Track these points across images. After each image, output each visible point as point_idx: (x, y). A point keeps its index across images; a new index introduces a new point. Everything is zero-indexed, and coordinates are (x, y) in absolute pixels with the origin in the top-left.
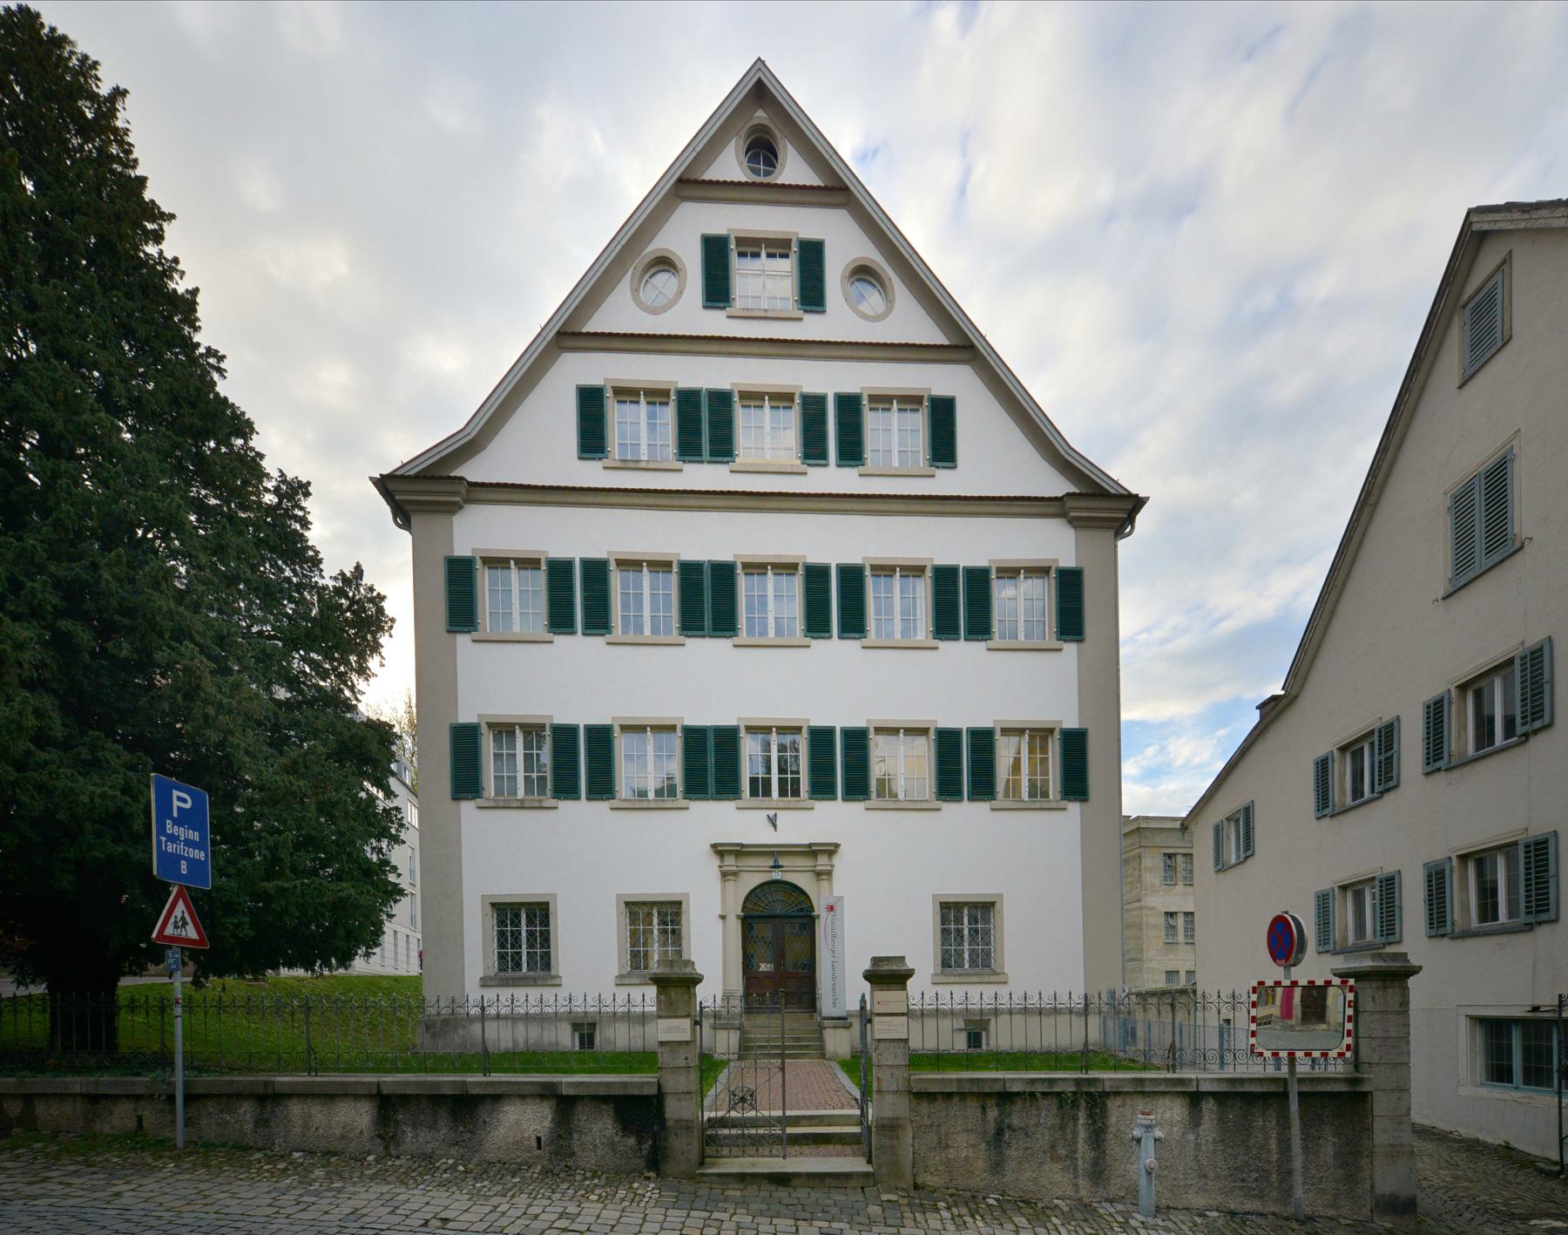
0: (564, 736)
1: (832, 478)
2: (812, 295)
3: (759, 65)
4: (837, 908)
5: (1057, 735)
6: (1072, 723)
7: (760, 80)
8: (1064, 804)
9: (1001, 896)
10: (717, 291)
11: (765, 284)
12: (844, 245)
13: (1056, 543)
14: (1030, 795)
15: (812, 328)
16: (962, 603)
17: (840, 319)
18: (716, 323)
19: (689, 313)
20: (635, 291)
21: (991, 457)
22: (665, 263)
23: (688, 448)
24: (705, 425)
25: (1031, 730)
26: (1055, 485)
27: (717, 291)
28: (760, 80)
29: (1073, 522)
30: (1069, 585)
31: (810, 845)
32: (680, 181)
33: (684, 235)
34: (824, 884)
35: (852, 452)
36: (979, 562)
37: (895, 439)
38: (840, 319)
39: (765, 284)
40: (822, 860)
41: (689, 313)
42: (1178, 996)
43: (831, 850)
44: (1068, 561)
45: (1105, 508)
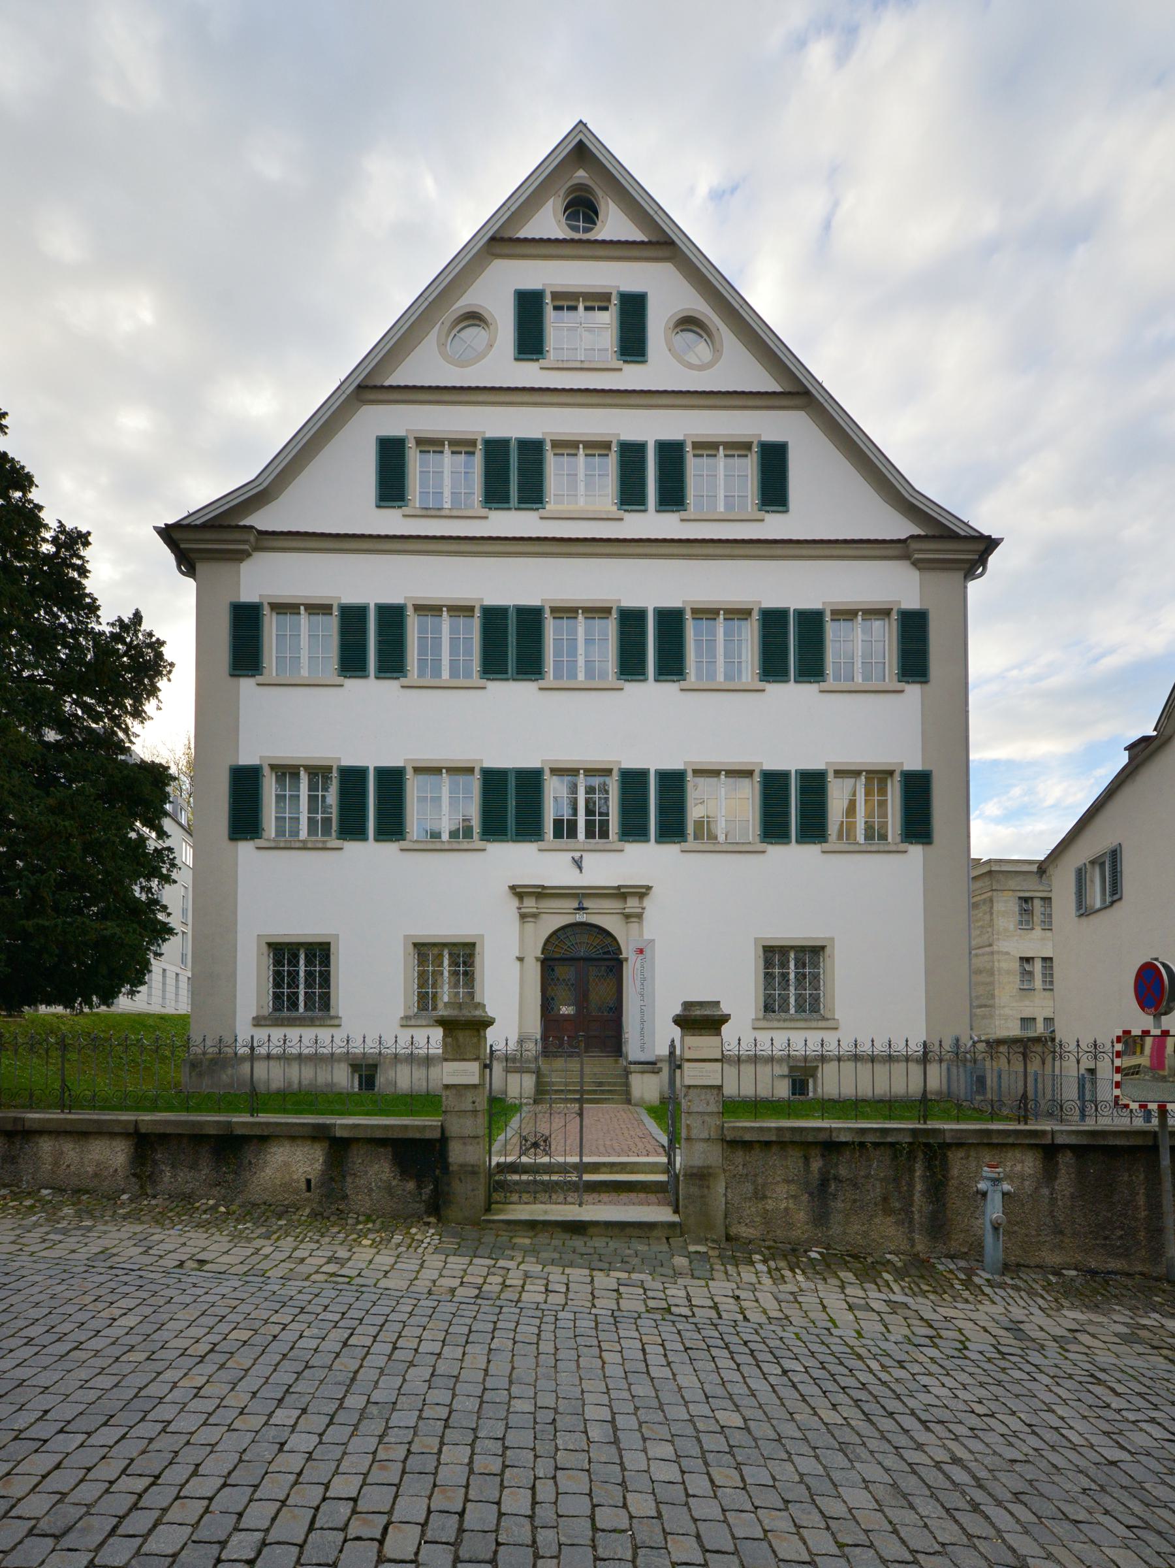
1: (651, 523)
2: (632, 344)
3: (581, 127)
4: (647, 951)
9: (832, 939)
10: (530, 343)
12: (666, 294)
13: (901, 586)
16: (792, 647)
18: (530, 374)
21: (823, 498)
22: (474, 318)
24: (514, 473)
25: (868, 772)
26: (900, 528)
29: (916, 564)
31: (619, 887)
33: (497, 288)
35: (673, 496)
38: (661, 369)
41: (500, 364)
43: (642, 892)
44: (912, 603)
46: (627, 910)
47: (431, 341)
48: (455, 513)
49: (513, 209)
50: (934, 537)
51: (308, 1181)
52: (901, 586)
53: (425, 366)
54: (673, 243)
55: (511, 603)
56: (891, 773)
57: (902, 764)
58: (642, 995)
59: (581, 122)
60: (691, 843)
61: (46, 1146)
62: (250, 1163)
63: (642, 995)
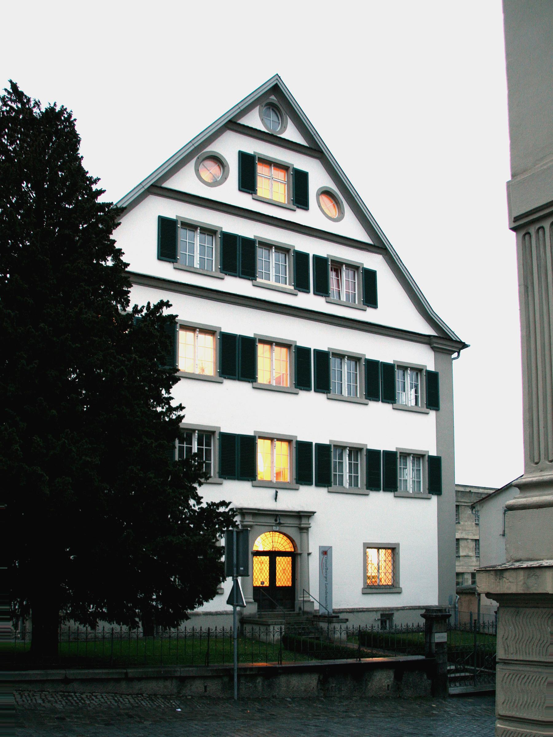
0: (373, 455)
1: (309, 301)
2: (300, 198)
3: (277, 77)
4: (328, 553)
5: (364, 453)
6: (433, 452)
7: (277, 84)
8: (297, 486)
9: (398, 544)
10: (248, 183)
11: (273, 187)
12: (318, 178)
13: (423, 357)
14: (350, 484)
15: (298, 216)
16: (380, 382)
17: (313, 216)
18: (245, 201)
19: (229, 192)
20: (197, 171)
21: (393, 306)
22: (217, 160)
23: (301, 285)
24: (239, 256)
25: (414, 454)
26: (426, 330)
27: (248, 183)
28: (277, 84)
29: (433, 348)
30: (432, 380)
31: (299, 512)
32: (230, 121)
33: (231, 147)
34: (305, 535)
35: (322, 289)
36: (324, 348)
37: (346, 285)
38: (313, 216)
39: (273, 187)
40: (304, 521)
41: (229, 192)
42: (80, 624)
43: (309, 515)
44: (431, 367)
45: (446, 343)
46: (302, 526)
47: (190, 167)
48: (201, 271)
49: (242, 108)
50: (443, 338)
51: (388, 685)
52: (423, 357)
53: (186, 181)
54: (322, 152)
55: (238, 334)
56: (423, 456)
57: (428, 452)
58: (326, 578)
59: (277, 74)
60: (333, 488)
61: (283, 679)
62: (366, 680)
63: (326, 578)
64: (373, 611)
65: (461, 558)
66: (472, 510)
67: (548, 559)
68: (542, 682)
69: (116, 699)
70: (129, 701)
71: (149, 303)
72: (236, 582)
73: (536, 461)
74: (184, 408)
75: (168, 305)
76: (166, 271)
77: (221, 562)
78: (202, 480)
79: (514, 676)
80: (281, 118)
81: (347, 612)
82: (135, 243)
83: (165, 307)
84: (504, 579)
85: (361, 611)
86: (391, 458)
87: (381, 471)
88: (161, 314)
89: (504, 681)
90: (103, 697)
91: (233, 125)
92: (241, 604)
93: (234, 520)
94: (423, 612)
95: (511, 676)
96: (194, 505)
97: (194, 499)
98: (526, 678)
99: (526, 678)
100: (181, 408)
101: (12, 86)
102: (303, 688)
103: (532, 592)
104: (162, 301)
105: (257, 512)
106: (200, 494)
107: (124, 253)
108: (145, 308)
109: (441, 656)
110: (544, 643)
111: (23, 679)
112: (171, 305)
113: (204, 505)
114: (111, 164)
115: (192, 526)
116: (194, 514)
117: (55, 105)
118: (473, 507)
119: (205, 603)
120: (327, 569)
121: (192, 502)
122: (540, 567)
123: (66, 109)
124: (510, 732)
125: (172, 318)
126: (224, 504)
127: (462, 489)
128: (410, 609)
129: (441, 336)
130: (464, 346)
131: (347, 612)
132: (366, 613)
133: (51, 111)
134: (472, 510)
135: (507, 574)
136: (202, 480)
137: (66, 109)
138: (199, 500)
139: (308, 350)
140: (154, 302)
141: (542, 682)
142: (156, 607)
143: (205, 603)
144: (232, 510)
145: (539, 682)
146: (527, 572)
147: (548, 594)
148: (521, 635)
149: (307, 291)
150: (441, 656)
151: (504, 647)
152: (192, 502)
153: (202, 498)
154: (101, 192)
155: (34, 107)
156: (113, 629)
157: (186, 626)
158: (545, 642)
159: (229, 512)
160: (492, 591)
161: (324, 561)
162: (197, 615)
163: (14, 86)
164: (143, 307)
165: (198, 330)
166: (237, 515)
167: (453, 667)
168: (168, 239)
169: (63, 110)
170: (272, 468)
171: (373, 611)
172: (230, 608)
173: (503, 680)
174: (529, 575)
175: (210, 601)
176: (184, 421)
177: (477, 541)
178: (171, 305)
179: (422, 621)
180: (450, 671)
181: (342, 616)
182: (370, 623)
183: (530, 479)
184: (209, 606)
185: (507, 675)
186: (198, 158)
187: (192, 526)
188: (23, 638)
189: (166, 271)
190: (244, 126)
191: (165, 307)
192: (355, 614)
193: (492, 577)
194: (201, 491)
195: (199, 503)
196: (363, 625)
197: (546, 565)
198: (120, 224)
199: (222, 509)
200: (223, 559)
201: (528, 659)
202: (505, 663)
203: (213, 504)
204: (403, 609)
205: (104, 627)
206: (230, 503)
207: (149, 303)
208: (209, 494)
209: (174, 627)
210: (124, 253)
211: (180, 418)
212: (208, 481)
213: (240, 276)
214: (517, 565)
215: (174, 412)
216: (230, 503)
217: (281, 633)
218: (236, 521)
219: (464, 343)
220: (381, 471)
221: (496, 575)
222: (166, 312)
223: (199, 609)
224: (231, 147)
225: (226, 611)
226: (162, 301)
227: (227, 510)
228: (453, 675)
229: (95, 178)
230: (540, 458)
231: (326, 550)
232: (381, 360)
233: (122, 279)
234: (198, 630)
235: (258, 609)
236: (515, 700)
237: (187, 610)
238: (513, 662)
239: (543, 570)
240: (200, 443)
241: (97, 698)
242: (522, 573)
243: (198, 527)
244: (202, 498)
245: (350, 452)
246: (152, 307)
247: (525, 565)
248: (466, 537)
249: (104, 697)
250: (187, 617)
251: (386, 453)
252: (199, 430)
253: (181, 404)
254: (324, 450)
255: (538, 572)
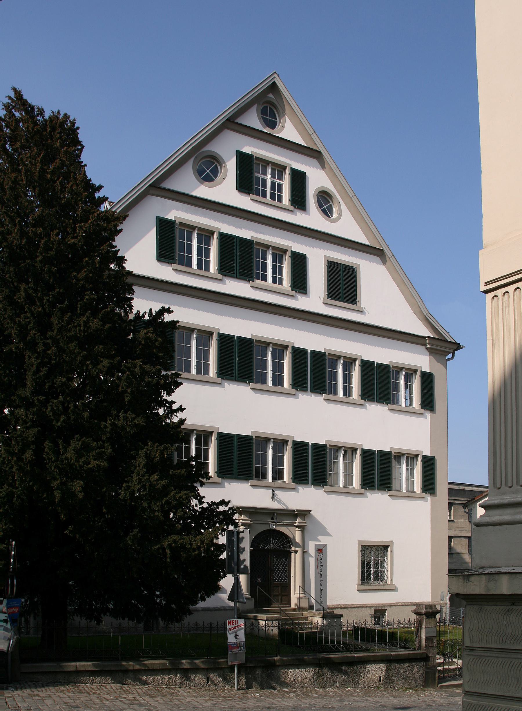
4: (324, 551)
6: (428, 453)
18: (244, 202)
30: (428, 379)
44: (427, 369)
64: (367, 607)
65: (454, 556)
66: (465, 509)
67: (505, 567)
68: (499, 664)
69: (124, 689)
70: (136, 691)
71: (151, 310)
72: (237, 580)
73: (498, 486)
74: (185, 409)
75: (169, 311)
76: (166, 273)
77: (222, 559)
78: (204, 480)
79: (477, 660)
80: (278, 114)
81: (341, 608)
82: (139, 254)
83: (166, 313)
84: (470, 583)
85: (355, 607)
86: (386, 458)
87: (378, 470)
88: (163, 320)
89: (470, 664)
90: (112, 688)
91: (232, 123)
92: (241, 600)
93: (234, 518)
94: (414, 608)
95: (474, 660)
96: (196, 505)
97: (196, 499)
98: (486, 661)
99: (486, 661)
100: (181, 409)
101: (16, 94)
102: (300, 679)
103: (491, 593)
104: (163, 308)
105: (254, 510)
106: (202, 494)
107: (126, 260)
108: (147, 314)
109: (431, 650)
110: (500, 634)
111: (37, 671)
112: (173, 311)
113: (205, 505)
114: (112, 167)
115: (193, 525)
116: (195, 513)
117: (59, 112)
118: (465, 506)
119: (207, 598)
120: (322, 566)
121: (194, 502)
122: (498, 573)
123: (69, 116)
124: (473, 704)
125: (173, 324)
126: (223, 502)
127: (456, 487)
128: (403, 605)
129: (437, 337)
130: (458, 347)
131: (341, 608)
132: (360, 609)
133: (55, 118)
134: (465, 509)
135: (472, 578)
136: (204, 480)
137: (68, 117)
138: (200, 499)
139: (304, 351)
140: (156, 308)
141: (499, 664)
142: (159, 604)
143: (207, 598)
144: (231, 508)
145: (496, 665)
146: (488, 576)
147: (503, 595)
148: (483, 626)
149: (304, 291)
150: (431, 650)
151: (470, 637)
152: (194, 502)
153: (204, 497)
154: (105, 199)
155: (38, 115)
156: (120, 624)
157: (188, 620)
158: (502, 632)
159: (228, 511)
160: (461, 592)
161: (319, 559)
162: (197, 610)
163: (18, 94)
164: (145, 313)
165: (196, 331)
166: (236, 513)
167: (442, 661)
168: (170, 242)
169: (66, 116)
170: (346, 607)
171: (367, 607)
172: (232, 604)
173: (468, 663)
174: (489, 579)
175: (212, 596)
176: (186, 422)
177: (469, 538)
178: (173, 311)
179: (413, 617)
180: (440, 664)
181: (336, 612)
182: (365, 619)
183: (493, 502)
184: (210, 602)
185: (472, 659)
186: (196, 157)
187: (193, 525)
188: (28, 633)
189: (166, 273)
190: (241, 125)
191: (166, 313)
192: (349, 609)
193: (461, 580)
194: (202, 491)
195: (201, 502)
196: (357, 621)
197: (502, 571)
198: (121, 230)
199: (222, 508)
200: (224, 556)
201: (488, 646)
202: (470, 650)
203: (214, 503)
204: (396, 605)
205: (112, 623)
206: (229, 502)
207: (151, 310)
208: (210, 494)
209: (177, 622)
210: (126, 260)
211: (182, 421)
212: (209, 481)
213: (238, 276)
214: (481, 571)
215: (175, 414)
216: (229, 502)
217: (279, 627)
218: (236, 519)
219: (459, 344)
220: (378, 470)
221: (464, 579)
222: (167, 318)
223: (201, 605)
224: (229, 149)
225: (224, 607)
226: (163, 308)
227: (227, 509)
228: (441, 668)
229: (97, 185)
230: (501, 484)
231: (321, 547)
232: (377, 361)
233: (125, 283)
234: (201, 625)
235: (255, 604)
236: (478, 679)
237: (189, 606)
238: (476, 649)
239: (501, 575)
240: (198, 443)
241: (106, 688)
242: (484, 578)
243: (199, 526)
244: (204, 497)
245: (345, 452)
246: (154, 314)
247: (486, 572)
248: (459, 535)
249: (113, 687)
250: (190, 613)
251: (381, 453)
252: (197, 430)
253: (181, 406)
254: (320, 450)
255: (496, 577)
